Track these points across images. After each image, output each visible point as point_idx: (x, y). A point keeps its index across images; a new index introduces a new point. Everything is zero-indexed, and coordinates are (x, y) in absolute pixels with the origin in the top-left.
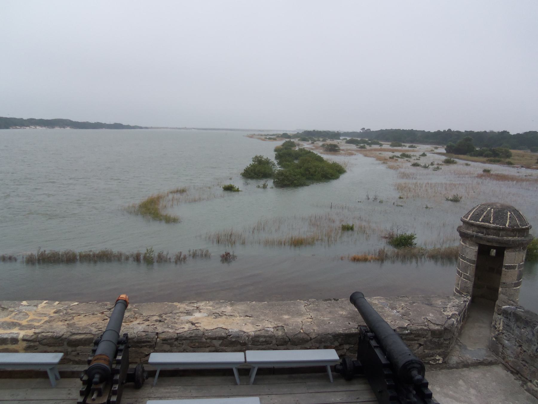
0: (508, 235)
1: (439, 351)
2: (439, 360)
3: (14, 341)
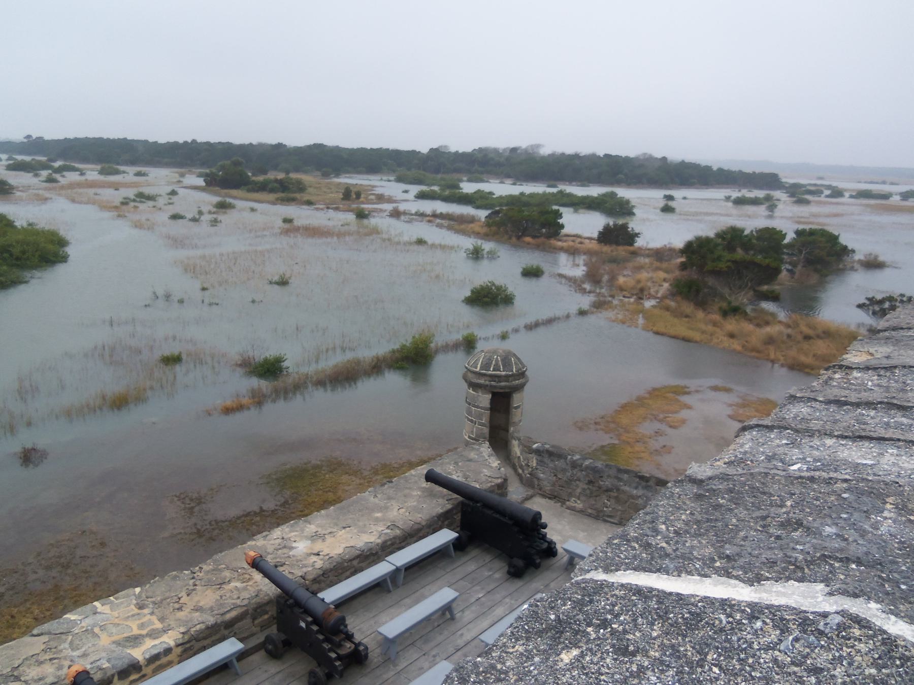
0: (515, 380)
3: (168, 651)
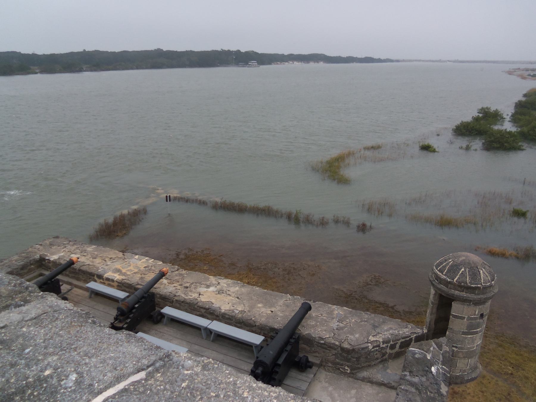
0: (455, 289)
1: (347, 364)
2: (347, 370)
